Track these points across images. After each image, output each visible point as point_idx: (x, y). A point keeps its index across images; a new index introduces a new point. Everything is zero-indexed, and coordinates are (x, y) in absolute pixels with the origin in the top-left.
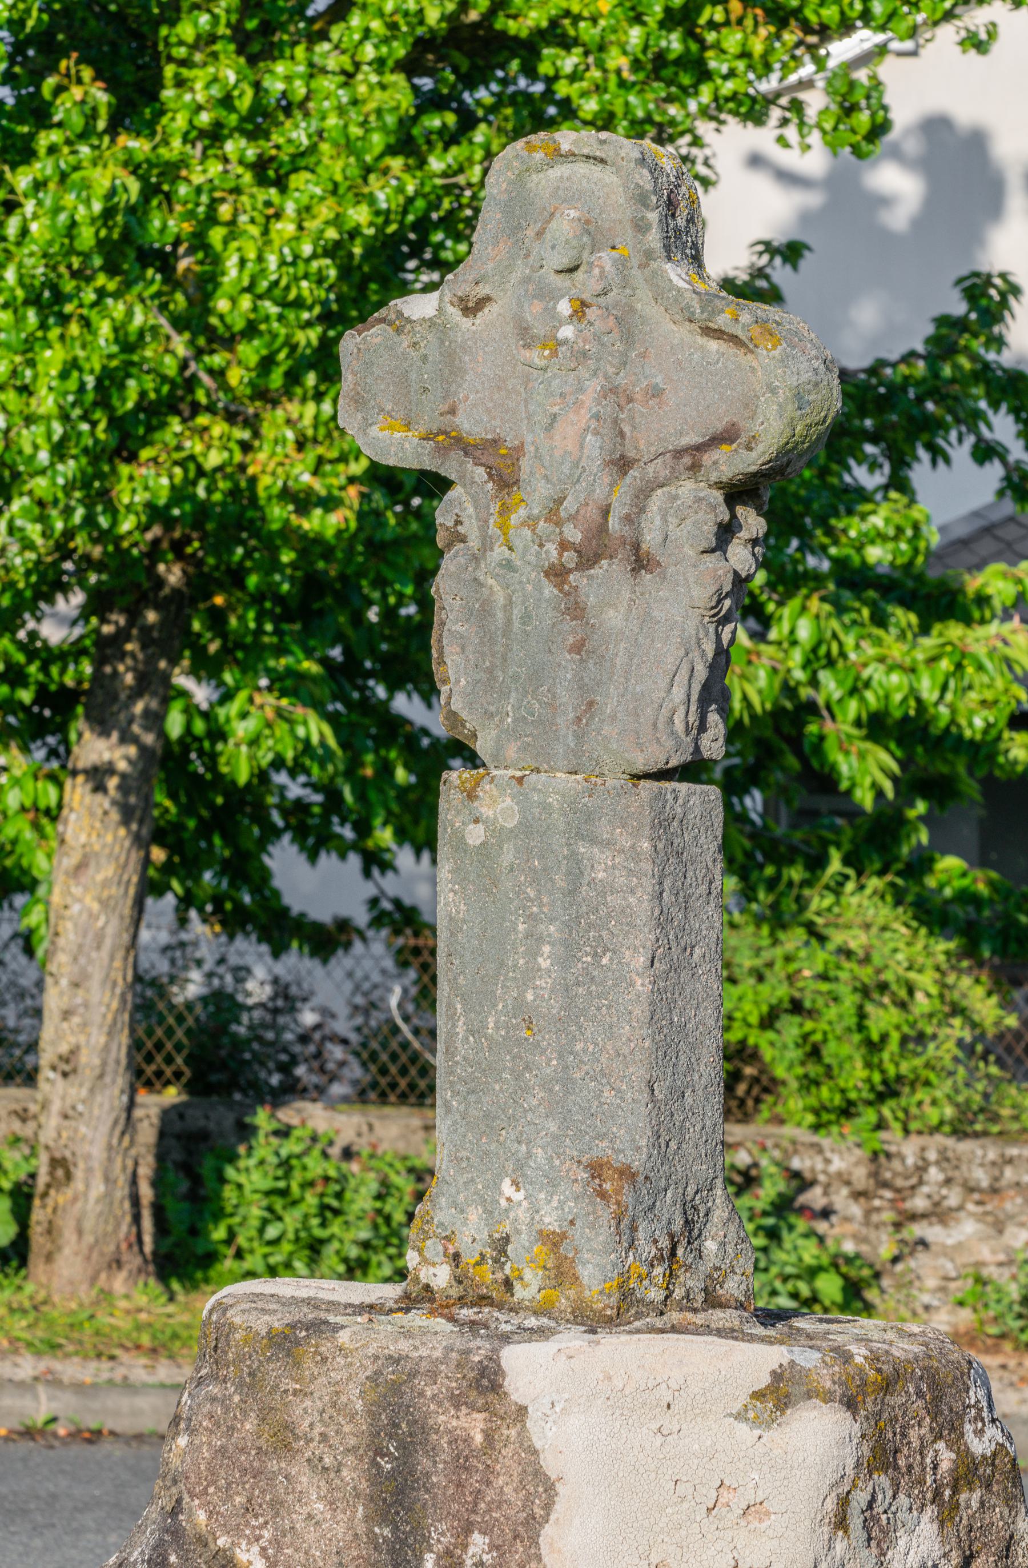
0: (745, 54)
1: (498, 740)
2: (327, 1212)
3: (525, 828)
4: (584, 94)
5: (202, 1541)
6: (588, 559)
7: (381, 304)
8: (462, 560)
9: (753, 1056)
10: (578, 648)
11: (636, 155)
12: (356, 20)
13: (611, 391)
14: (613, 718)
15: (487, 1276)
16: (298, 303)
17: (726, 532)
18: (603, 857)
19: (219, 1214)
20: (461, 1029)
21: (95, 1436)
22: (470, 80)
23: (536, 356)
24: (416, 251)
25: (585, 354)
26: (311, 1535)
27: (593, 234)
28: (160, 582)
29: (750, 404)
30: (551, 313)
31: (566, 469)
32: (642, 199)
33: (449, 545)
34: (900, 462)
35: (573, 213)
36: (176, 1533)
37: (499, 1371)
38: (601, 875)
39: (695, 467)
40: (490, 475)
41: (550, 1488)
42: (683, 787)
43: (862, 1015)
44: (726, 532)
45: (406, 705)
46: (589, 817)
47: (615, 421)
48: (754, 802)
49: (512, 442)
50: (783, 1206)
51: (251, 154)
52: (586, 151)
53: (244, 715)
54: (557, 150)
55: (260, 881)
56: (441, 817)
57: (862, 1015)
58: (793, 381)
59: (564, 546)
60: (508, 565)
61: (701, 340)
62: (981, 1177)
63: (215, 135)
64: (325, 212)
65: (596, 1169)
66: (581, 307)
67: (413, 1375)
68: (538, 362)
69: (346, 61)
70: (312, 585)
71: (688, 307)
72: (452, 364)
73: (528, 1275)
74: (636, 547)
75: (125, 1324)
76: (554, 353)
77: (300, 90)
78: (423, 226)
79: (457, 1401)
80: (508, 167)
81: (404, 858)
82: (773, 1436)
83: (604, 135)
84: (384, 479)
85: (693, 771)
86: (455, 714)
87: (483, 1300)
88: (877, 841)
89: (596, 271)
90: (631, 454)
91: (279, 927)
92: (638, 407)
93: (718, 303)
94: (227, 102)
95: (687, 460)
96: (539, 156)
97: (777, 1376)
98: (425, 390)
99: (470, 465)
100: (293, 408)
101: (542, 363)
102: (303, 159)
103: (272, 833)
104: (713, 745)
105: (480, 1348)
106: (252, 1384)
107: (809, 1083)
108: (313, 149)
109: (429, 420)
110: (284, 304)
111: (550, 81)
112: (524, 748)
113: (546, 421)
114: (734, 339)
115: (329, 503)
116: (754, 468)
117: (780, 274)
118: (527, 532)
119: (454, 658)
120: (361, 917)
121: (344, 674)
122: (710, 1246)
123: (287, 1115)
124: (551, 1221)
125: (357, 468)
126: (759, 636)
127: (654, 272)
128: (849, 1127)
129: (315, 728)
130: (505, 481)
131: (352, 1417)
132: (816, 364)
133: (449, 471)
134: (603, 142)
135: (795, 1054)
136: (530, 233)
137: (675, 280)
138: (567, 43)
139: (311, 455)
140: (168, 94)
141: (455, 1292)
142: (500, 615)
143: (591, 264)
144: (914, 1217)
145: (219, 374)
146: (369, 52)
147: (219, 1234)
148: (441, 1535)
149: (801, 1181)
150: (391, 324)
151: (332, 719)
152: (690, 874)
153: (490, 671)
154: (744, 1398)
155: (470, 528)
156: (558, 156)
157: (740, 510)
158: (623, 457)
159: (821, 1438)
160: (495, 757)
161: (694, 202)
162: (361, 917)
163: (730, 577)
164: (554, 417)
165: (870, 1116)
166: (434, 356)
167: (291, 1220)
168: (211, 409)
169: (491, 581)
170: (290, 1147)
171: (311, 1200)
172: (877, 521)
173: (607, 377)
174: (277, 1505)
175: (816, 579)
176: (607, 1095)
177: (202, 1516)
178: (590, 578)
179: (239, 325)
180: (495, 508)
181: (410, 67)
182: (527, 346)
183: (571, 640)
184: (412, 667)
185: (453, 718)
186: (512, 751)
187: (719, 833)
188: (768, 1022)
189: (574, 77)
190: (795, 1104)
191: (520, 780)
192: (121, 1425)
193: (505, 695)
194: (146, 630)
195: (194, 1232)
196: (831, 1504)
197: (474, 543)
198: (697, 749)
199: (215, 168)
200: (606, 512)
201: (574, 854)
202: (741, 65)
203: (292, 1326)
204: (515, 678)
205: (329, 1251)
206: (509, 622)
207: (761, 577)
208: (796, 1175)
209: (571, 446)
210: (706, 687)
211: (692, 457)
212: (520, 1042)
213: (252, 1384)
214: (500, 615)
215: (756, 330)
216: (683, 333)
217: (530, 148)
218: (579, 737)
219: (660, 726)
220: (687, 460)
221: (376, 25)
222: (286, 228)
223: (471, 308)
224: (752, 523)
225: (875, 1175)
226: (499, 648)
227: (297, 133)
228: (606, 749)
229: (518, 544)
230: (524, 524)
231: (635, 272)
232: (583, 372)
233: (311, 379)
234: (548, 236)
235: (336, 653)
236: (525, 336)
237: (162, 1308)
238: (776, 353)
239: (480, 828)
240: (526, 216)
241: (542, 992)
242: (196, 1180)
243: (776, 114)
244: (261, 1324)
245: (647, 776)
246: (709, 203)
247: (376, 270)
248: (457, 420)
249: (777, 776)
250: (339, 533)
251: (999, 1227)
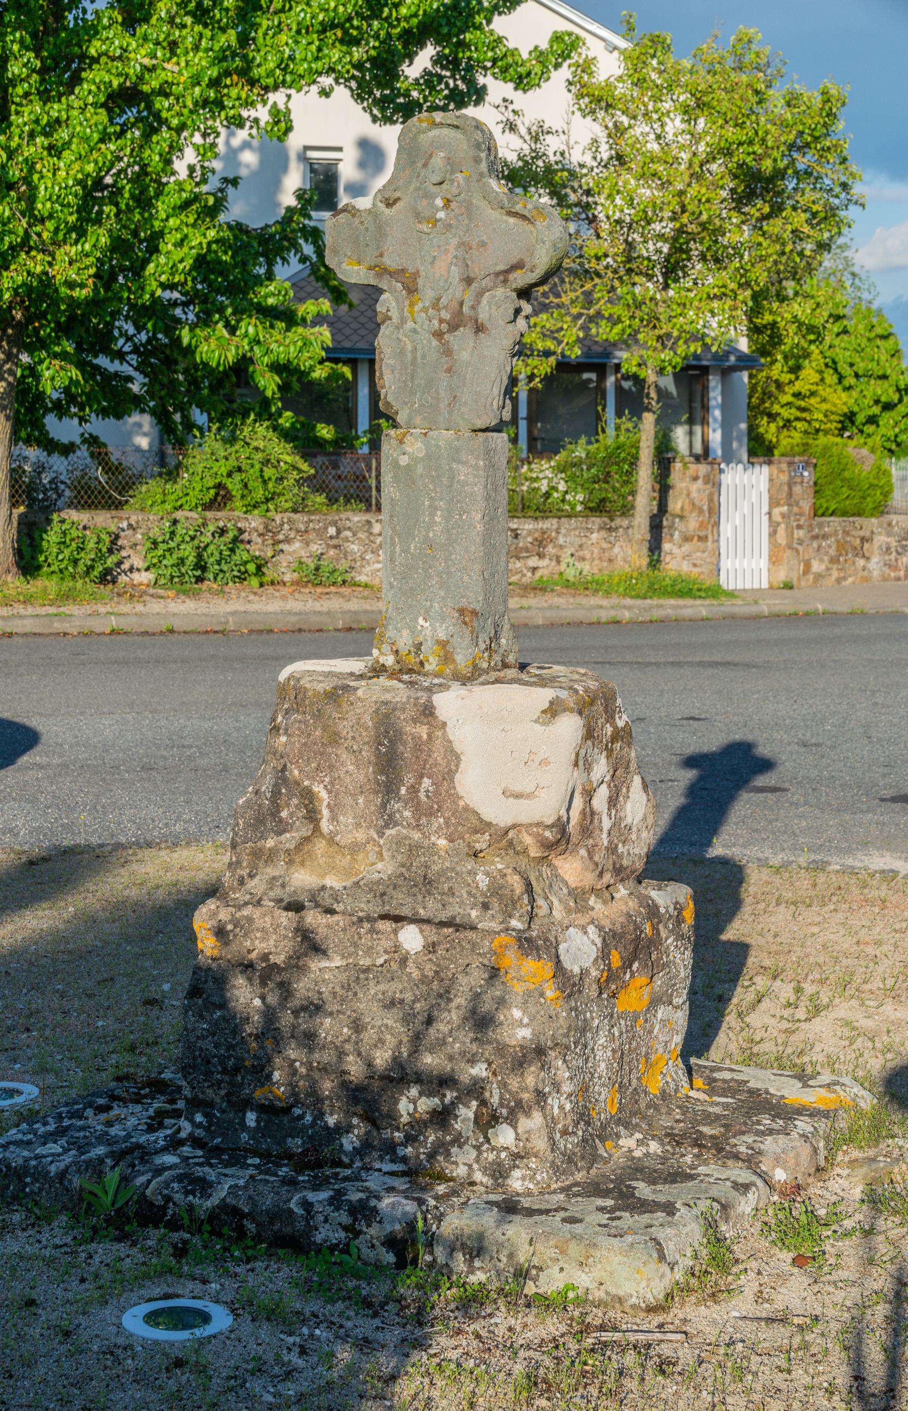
0: (239, 98)
1: (410, 416)
2: (80, 549)
3: (428, 457)
5: (297, 783)
6: (454, 327)
9: (225, 487)
10: (449, 370)
13: (462, 244)
15: (412, 660)
16: (69, 205)
17: (518, 311)
19: (42, 552)
20: (398, 549)
21: (10, 635)
23: (425, 227)
26: (348, 780)
27: (453, 165)
28: (13, 318)
29: (531, 250)
30: (432, 205)
31: (441, 283)
34: (270, 264)
36: (285, 780)
37: (433, 707)
39: (505, 281)
41: (458, 758)
42: (495, 434)
43: (262, 471)
46: (457, 451)
49: (411, 270)
50: (235, 540)
51: (46, 143)
53: (48, 369)
55: (41, 428)
57: (262, 471)
58: (552, 238)
59: (441, 321)
60: (415, 331)
61: (505, 218)
62: (302, 527)
63: (32, 135)
64: (76, 166)
65: (462, 611)
66: (448, 202)
67: (394, 709)
69: (81, 103)
70: (72, 318)
73: (431, 659)
75: (13, 592)
77: (64, 116)
79: (415, 721)
82: (551, 728)
87: (411, 671)
88: (264, 409)
91: (51, 446)
94: (37, 121)
95: (501, 278)
96: (424, 125)
97: (551, 703)
100: (67, 248)
102: (67, 145)
105: (423, 697)
106: (319, 715)
107: (243, 496)
109: (370, 260)
110: (62, 205)
112: (424, 419)
114: (524, 217)
115: (82, 286)
120: (78, 441)
122: (503, 641)
123: (64, 515)
124: (442, 636)
128: (256, 512)
129: (75, 373)
130: (411, 290)
131: (367, 729)
133: (383, 285)
135: (239, 486)
136: (419, 165)
138: (167, 96)
139: (76, 266)
140: (13, 118)
141: (397, 667)
142: (409, 355)
144: (280, 542)
145: (39, 235)
146: (90, 99)
147: (42, 558)
148: (409, 779)
149: (241, 531)
154: (538, 713)
155: (394, 314)
156: (434, 125)
159: (569, 727)
162: (78, 441)
165: (264, 507)
166: (372, 228)
167: (67, 552)
168: (36, 249)
170: (65, 526)
171: (74, 545)
172: (272, 288)
174: (331, 767)
176: (466, 578)
177: (296, 772)
179: (46, 214)
180: (407, 303)
188: (229, 475)
190: (238, 503)
192: (19, 630)
194: (9, 336)
195: (33, 558)
196: (573, 757)
199: (32, 149)
200: (461, 304)
203: (335, 688)
205: (81, 563)
208: (240, 529)
212: (426, 556)
213: (319, 715)
220: (501, 278)
222: (62, 174)
225: (266, 527)
227: (63, 134)
229: (419, 320)
232: (448, 235)
236: (418, 216)
237: (25, 586)
241: (436, 533)
242: (32, 539)
244: (320, 687)
251: (308, 544)
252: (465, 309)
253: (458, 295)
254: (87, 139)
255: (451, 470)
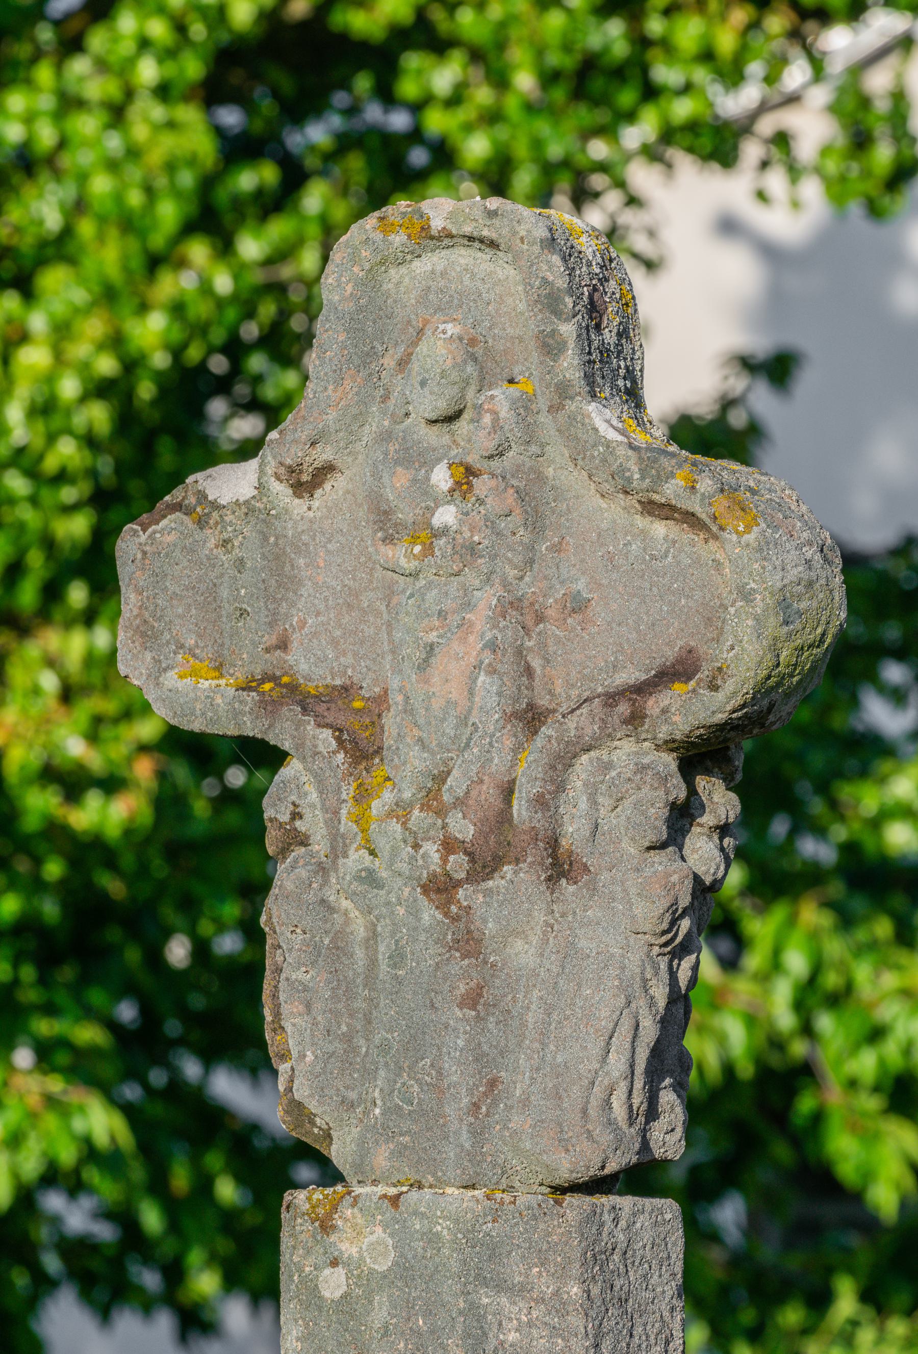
1: (361, 1142)
3: (404, 1271)
4: (468, 128)
6: (484, 865)
7: (177, 479)
8: (303, 873)
10: (472, 1000)
11: (542, 232)
12: (127, 22)
13: (512, 605)
14: (525, 1102)
17: (682, 816)
18: (514, 1310)
22: (300, 109)
23: (401, 555)
24: (223, 386)
25: (472, 549)
27: (481, 360)
29: (713, 620)
30: (422, 486)
32: (550, 303)
33: (284, 851)
35: (451, 329)
38: (512, 1337)
39: (635, 719)
40: (339, 740)
42: (626, 1202)
44: (682, 816)
45: (228, 1087)
46: (494, 1252)
47: (520, 652)
48: (729, 1214)
52: (468, 229)
54: (425, 228)
56: (285, 1258)
58: (775, 581)
59: (449, 846)
60: (370, 879)
61: (641, 522)
64: (94, 327)
68: (405, 564)
71: (622, 469)
72: (279, 571)
74: (553, 843)
76: (429, 550)
77: (46, 136)
78: (235, 348)
80: (354, 258)
81: (236, 1315)
83: (494, 203)
84: (190, 749)
85: (641, 1178)
86: (300, 1105)
89: (487, 419)
90: (543, 702)
92: (551, 628)
93: (665, 462)
95: (624, 708)
96: (398, 239)
98: (243, 613)
99: (311, 728)
100: (51, 639)
101: (412, 565)
103: (43, 1284)
104: (669, 1139)
108: (67, 232)
109: (249, 660)
111: (417, 108)
112: (400, 1153)
113: (420, 654)
114: (690, 519)
115: (112, 784)
116: (720, 717)
117: (763, 401)
118: (395, 827)
119: (294, 1018)
121: (139, 1047)
125: (147, 730)
126: (730, 964)
127: (572, 418)
129: (101, 1122)
130: (362, 750)
132: (810, 552)
134: (492, 214)
136: (389, 362)
137: (602, 427)
138: (439, 46)
142: (360, 953)
143: (478, 408)
146: (148, 71)
150: (189, 512)
151: (129, 1111)
152: (638, 1330)
153: (348, 1038)
155: (313, 824)
156: (427, 238)
157: (701, 782)
158: (531, 706)
160: (359, 1167)
161: (628, 304)
163: (689, 884)
164: (431, 648)
169: (345, 904)
173: (505, 584)
175: (810, 878)
178: (488, 893)
180: (348, 791)
181: (211, 93)
182: (388, 540)
183: (462, 988)
184: (239, 1038)
185: (296, 1108)
186: (381, 1158)
187: (679, 1268)
189: (455, 100)
191: (395, 1201)
193: (369, 1074)
197: (320, 846)
198: (645, 1146)
200: (508, 791)
201: (473, 1306)
202: (701, 75)
204: (384, 1048)
206: (373, 963)
207: (736, 877)
209: (456, 692)
210: (656, 1052)
211: (630, 703)
214: (360, 953)
215: (721, 504)
216: (614, 512)
217: (385, 226)
218: (477, 1134)
219: (592, 1112)
220: (624, 708)
221: (158, 29)
223: (306, 483)
224: (720, 801)
226: (359, 1004)
228: (516, 1150)
229: (383, 845)
230: (390, 814)
231: (544, 418)
232: (471, 578)
233: (77, 595)
234: (415, 366)
235: (127, 1012)
236: (385, 523)
238: (751, 538)
239: (340, 1271)
240: (382, 335)
243: (752, 151)
245: (575, 1188)
246: (651, 297)
247: (160, 433)
248: (290, 658)
249: (762, 1175)
250: (128, 832)
252: (520, 809)
253: (498, 763)
254: (129, 224)
255: (474, 1312)
